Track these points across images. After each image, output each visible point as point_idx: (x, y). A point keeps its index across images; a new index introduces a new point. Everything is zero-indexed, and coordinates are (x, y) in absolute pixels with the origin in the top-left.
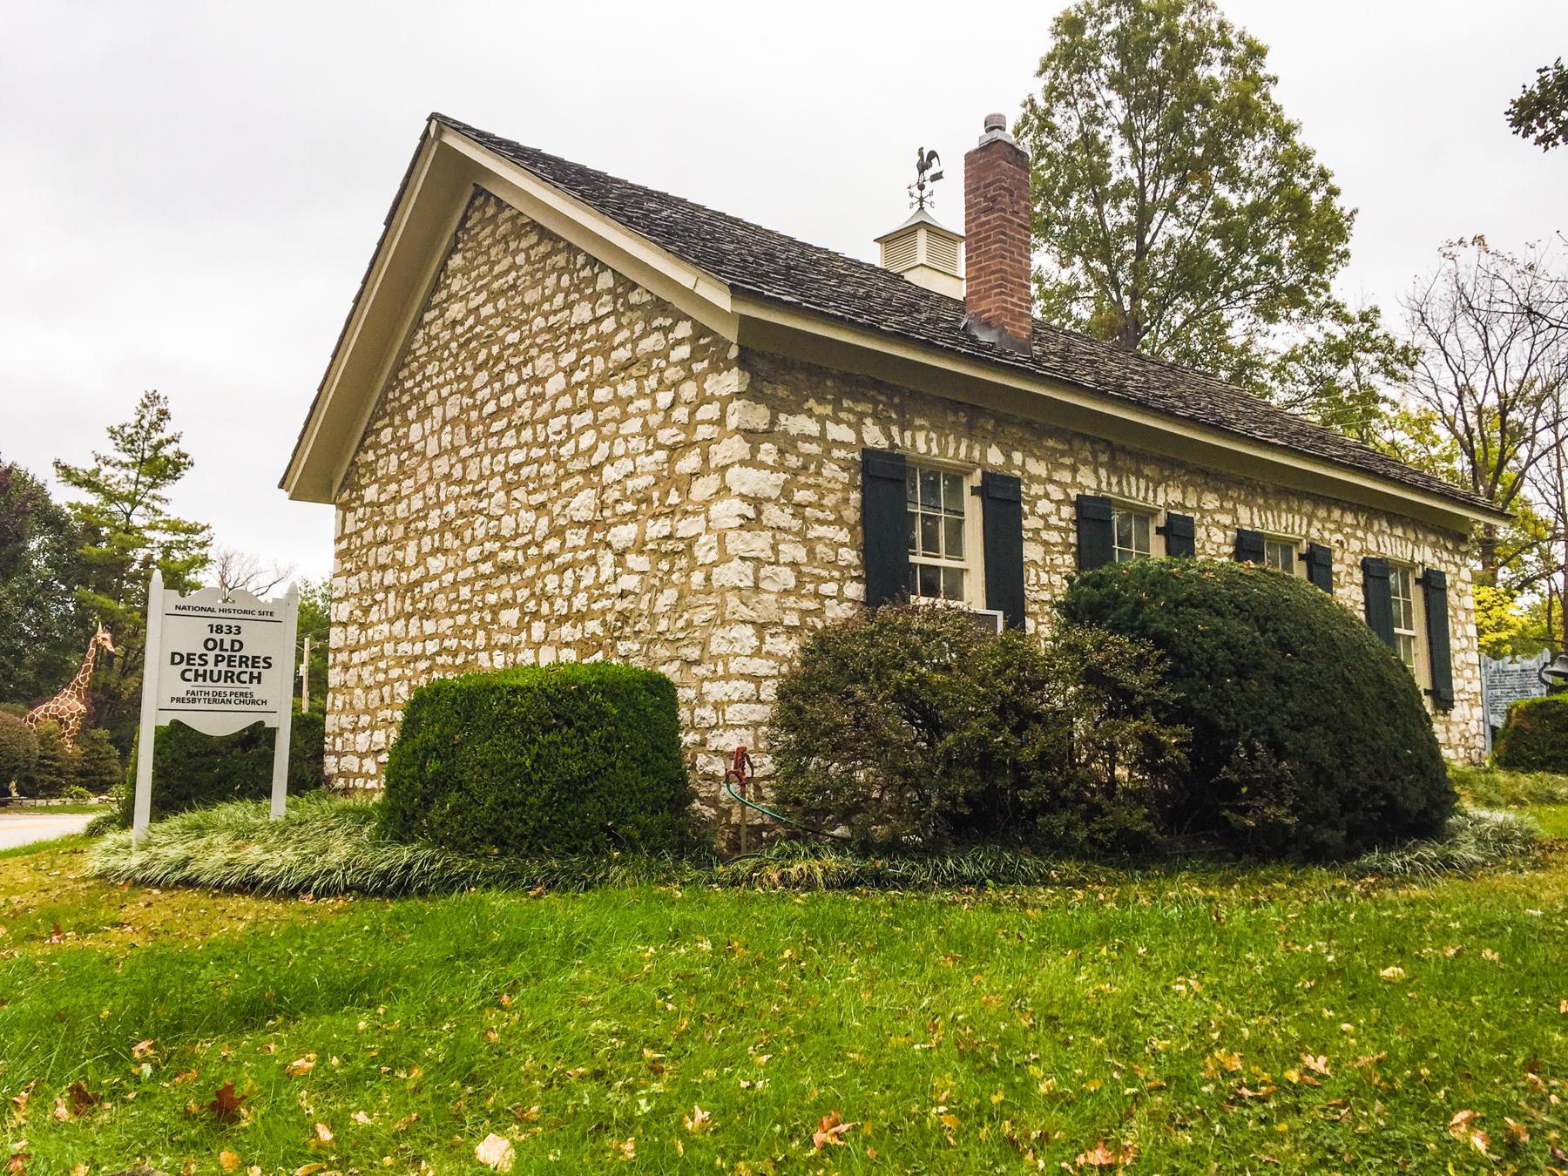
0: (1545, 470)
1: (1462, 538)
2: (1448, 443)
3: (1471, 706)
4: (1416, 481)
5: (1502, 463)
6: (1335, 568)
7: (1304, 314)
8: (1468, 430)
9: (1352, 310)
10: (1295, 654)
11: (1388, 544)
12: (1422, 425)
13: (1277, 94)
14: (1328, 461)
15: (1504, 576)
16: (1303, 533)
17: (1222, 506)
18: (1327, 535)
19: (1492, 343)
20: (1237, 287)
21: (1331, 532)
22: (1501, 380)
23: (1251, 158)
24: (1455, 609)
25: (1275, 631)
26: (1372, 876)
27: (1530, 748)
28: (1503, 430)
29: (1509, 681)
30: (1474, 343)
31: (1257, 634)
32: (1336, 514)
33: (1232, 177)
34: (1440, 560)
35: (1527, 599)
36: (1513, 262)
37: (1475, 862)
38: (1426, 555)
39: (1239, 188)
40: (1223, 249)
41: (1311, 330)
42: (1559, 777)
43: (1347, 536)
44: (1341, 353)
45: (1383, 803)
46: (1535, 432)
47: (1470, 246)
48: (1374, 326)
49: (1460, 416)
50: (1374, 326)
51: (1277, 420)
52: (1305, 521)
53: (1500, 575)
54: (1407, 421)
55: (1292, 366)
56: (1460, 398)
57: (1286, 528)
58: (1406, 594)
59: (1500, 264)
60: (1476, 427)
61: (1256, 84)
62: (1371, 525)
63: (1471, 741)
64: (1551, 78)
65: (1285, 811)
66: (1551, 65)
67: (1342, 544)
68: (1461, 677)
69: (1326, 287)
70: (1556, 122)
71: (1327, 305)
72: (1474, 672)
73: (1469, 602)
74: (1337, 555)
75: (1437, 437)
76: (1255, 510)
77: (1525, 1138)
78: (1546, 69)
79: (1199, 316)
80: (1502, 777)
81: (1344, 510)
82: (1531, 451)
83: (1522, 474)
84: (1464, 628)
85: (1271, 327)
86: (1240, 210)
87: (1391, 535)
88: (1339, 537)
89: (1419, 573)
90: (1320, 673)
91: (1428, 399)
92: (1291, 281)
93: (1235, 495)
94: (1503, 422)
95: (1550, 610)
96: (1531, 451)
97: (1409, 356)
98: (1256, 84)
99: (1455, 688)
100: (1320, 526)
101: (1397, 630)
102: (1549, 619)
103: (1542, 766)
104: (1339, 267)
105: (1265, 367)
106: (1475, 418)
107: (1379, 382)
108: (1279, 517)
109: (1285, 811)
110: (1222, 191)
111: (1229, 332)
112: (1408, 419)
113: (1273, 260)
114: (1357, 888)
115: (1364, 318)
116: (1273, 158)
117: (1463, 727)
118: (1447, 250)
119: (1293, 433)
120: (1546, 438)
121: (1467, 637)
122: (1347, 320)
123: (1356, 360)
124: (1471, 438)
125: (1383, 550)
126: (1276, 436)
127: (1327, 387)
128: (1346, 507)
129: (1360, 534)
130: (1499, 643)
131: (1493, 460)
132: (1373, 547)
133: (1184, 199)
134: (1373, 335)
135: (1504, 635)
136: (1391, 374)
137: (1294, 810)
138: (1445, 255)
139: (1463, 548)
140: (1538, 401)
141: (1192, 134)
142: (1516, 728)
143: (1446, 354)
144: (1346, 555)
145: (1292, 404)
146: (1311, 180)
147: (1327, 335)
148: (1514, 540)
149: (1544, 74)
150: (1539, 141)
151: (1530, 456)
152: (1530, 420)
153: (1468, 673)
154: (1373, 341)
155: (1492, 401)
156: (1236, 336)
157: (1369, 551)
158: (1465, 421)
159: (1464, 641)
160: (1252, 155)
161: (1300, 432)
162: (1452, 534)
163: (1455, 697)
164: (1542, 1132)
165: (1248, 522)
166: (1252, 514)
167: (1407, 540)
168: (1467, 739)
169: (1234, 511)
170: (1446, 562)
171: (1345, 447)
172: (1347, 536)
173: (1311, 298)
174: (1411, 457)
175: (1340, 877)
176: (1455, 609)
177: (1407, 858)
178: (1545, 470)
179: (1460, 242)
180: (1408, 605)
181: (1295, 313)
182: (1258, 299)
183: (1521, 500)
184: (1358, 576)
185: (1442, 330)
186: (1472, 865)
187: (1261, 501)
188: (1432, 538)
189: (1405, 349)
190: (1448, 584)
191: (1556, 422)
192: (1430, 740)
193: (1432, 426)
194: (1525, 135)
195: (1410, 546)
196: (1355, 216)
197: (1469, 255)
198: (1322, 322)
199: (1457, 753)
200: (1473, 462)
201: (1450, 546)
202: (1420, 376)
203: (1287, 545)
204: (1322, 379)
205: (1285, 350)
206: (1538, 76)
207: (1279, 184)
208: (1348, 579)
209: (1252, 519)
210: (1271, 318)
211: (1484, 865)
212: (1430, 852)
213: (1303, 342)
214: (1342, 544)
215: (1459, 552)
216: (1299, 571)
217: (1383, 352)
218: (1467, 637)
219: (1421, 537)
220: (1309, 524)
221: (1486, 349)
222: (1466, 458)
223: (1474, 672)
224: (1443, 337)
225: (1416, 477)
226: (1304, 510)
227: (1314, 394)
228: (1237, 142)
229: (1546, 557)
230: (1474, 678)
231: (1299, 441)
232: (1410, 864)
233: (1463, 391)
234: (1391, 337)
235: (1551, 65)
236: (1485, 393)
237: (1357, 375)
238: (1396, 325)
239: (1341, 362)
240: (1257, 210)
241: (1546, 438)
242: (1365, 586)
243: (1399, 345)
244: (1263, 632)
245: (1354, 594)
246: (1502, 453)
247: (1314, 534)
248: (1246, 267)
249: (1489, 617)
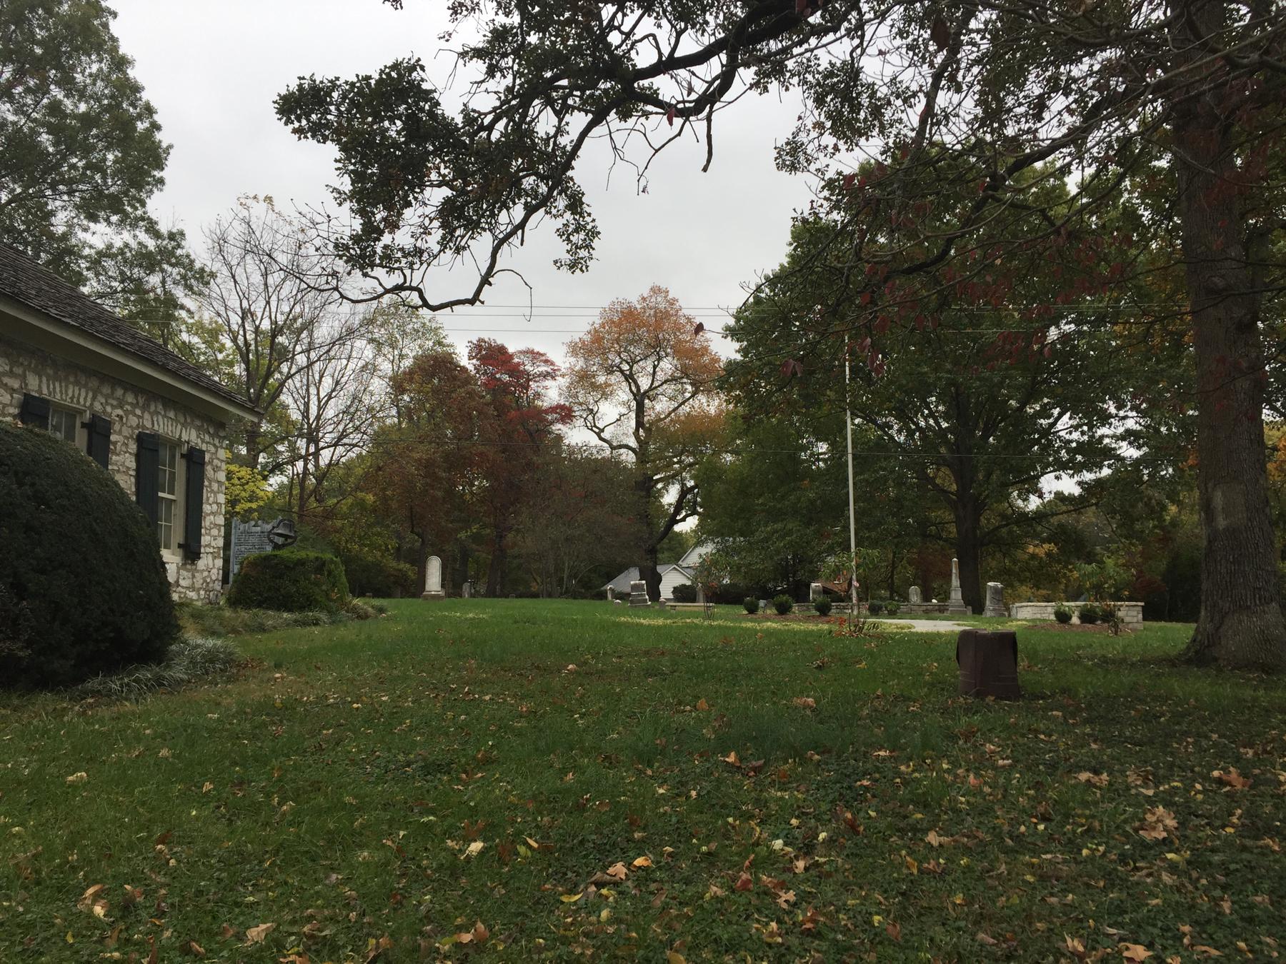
0: (298, 385)
1: (221, 426)
2: (231, 351)
3: (214, 558)
4: (189, 375)
5: (269, 374)
6: (113, 438)
7: (122, 221)
8: (247, 344)
9: (163, 228)
10: (49, 507)
11: (161, 424)
12: (211, 335)
13: (115, 27)
14: (115, 346)
15: (263, 461)
16: (88, 404)
17: (11, 371)
18: (109, 409)
19: (270, 280)
20: (63, 182)
21: (113, 407)
22: (274, 310)
23: (87, 73)
24: (210, 481)
25: (33, 485)
26: (92, 697)
27: (253, 591)
28: (272, 348)
29: (252, 540)
30: (257, 278)
31: (14, 487)
32: (119, 392)
33: (67, 83)
34: (203, 441)
35: (276, 480)
36: (290, 224)
37: (182, 680)
38: (191, 436)
39: (73, 96)
40: (55, 145)
41: (126, 236)
42: (270, 612)
43: (127, 412)
44: (149, 261)
45: (112, 635)
46: (294, 355)
47: (261, 202)
48: (179, 246)
49: (241, 332)
50: (179, 246)
51: (78, 304)
52: (90, 395)
53: (261, 460)
54: (199, 328)
55: (108, 263)
56: (243, 319)
57: (72, 398)
58: (172, 465)
59: (281, 222)
60: (252, 342)
61: (97, 13)
62: (149, 406)
63: (211, 585)
64: (306, 86)
65: (20, 644)
66: (307, 77)
67: (121, 418)
68: (209, 534)
69: (143, 204)
70: (308, 121)
71: (143, 219)
72: (219, 531)
73: (222, 476)
74: (117, 427)
75: (223, 345)
76: (44, 379)
77: (140, 899)
78: (304, 78)
79: (24, 199)
80: (228, 613)
81: (126, 390)
82: (290, 369)
83: (282, 384)
84: (215, 496)
85: (92, 225)
86: (74, 116)
87: (164, 416)
88: (120, 412)
89: (185, 449)
90: (70, 524)
91: (219, 315)
92: (112, 189)
93: (26, 363)
94: (273, 342)
95: (291, 488)
96: (290, 369)
97: (204, 277)
98: (97, 13)
99: (203, 543)
100: (103, 401)
101: (161, 494)
102: (291, 494)
103: (259, 605)
104: (155, 190)
105: (82, 257)
106: (253, 336)
107: (179, 293)
108: (67, 387)
109: (20, 644)
110: (58, 93)
111: (53, 220)
112: (202, 328)
113: (99, 167)
114: (77, 708)
115: (172, 236)
116: (107, 79)
117: (206, 574)
118: (243, 201)
119: (89, 318)
120: (301, 360)
121: (217, 504)
122: (157, 235)
123: (163, 271)
124: (248, 351)
125: (156, 427)
126: (71, 316)
127: (139, 288)
128: (128, 387)
129: (138, 412)
130: (250, 510)
131: (263, 371)
132: (149, 425)
133: (20, 89)
134: (179, 252)
135: (254, 506)
136: (189, 288)
137: (29, 644)
138: (241, 204)
139: (222, 434)
140: (300, 331)
141: (33, 34)
142: (246, 575)
143: (235, 282)
144: (124, 428)
145: (101, 295)
146: (138, 110)
147: (139, 243)
148: (272, 433)
149: (302, 82)
150: (295, 131)
151: (289, 372)
152: (291, 346)
153: (215, 532)
154: (176, 258)
155: (266, 325)
156: (59, 223)
157: (144, 427)
158: (245, 336)
159: (215, 506)
160: (88, 71)
161: (97, 318)
162: (214, 422)
163: (202, 550)
164: (155, 891)
165: (36, 388)
166: (41, 381)
167: (177, 421)
168: (208, 583)
169: (23, 378)
170: (207, 443)
171: (135, 338)
172: (127, 412)
173: (129, 209)
174: (202, 358)
175: (63, 700)
176: (210, 481)
177: (126, 680)
178: (298, 385)
179: (255, 197)
180: (172, 475)
181: (114, 218)
182: (82, 198)
183: (281, 404)
184: (133, 447)
185: (234, 262)
186: (180, 682)
187: (50, 372)
188: (198, 423)
189: (202, 270)
190: (207, 459)
191: (308, 351)
192: (161, 583)
193: (221, 337)
194: (286, 124)
195: (179, 427)
196: (171, 151)
197: (259, 209)
198: (137, 232)
199: (199, 595)
200: (247, 370)
201: (212, 431)
202: (214, 295)
203: (72, 414)
204: (131, 279)
205: (101, 246)
206: (298, 82)
207: (109, 105)
208: (124, 449)
209: (40, 386)
210: (93, 218)
211: (189, 682)
212: (146, 674)
213: (118, 243)
214: (121, 418)
215: (220, 437)
216: (81, 439)
217: (184, 268)
218: (217, 504)
219: (189, 420)
220: (94, 398)
221: (266, 284)
222: (243, 366)
223: (219, 531)
224: (234, 268)
225: (191, 372)
226: (90, 385)
227: (123, 290)
228: (75, 54)
229: (292, 448)
230: (219, 536)
231: (92, 325)
232: (128, 685)
233: (246, 314)
234: (192, 257)
235: (307, 77)
236: (262, 319)
237: (163, 282)
238: (197, 248)
239: (151, 269)
240: (87, 121)
241: (301, 360)
242: (138, 456)
243: (197, 265)
244: (21, 484)
245: (128, 461)
246: (269, 368)
247: (98, 407)
248: (73, 167)
249: (245, 490)
